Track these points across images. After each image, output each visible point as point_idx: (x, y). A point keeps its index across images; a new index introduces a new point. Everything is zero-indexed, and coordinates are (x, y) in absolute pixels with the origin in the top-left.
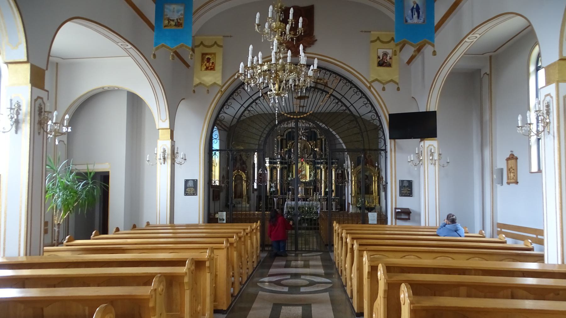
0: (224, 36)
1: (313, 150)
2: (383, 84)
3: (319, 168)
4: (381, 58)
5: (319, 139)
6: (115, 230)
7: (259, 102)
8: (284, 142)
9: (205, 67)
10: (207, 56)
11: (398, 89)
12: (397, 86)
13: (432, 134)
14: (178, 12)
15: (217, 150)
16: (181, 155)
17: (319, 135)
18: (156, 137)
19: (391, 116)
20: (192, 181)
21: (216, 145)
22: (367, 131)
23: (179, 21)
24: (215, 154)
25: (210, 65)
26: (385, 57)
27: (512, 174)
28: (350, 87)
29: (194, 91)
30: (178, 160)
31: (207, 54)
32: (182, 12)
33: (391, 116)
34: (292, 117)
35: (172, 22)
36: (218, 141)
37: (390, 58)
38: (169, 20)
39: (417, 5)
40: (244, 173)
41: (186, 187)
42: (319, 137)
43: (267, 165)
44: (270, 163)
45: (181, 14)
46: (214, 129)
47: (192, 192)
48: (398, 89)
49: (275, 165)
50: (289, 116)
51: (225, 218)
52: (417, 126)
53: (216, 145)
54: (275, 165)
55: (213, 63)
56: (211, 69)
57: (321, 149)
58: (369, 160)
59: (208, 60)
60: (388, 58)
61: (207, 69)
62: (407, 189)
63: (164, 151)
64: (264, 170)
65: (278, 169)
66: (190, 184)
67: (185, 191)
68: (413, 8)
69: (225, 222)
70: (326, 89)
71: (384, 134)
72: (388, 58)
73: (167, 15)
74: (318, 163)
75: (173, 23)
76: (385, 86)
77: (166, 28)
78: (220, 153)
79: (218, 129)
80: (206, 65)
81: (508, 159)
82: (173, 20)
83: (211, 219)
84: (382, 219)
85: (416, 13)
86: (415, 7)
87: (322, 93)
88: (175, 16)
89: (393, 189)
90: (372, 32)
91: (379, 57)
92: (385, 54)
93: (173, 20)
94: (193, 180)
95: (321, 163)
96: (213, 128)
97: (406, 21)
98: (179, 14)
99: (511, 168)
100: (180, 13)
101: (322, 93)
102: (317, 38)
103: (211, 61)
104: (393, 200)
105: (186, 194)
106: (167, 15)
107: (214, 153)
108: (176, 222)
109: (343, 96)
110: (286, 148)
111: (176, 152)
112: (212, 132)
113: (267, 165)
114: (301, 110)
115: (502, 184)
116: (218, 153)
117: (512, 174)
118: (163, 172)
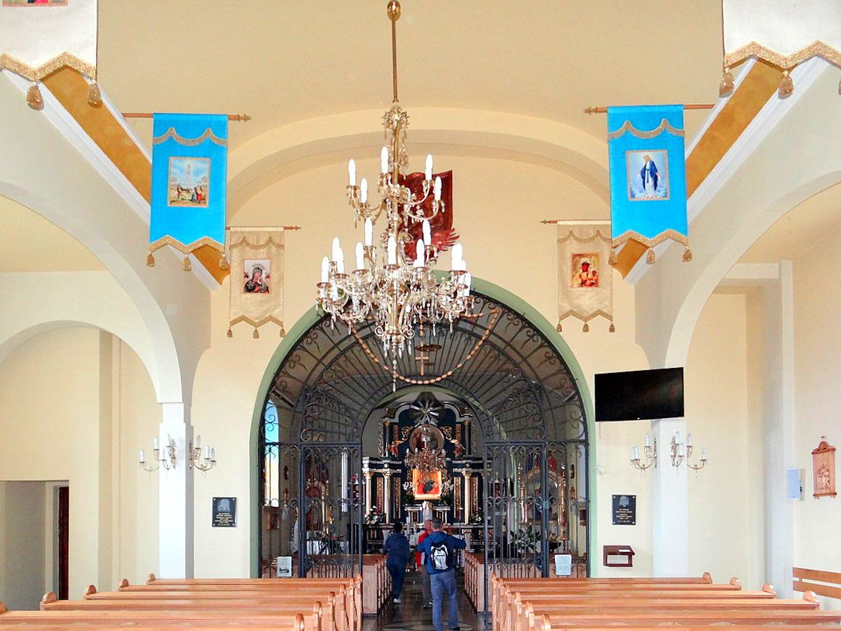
0: (285, 228)
1: (447, 442)
2: (586, 319)
3: (459, 475)
4: (251, 277)
5: (459, 423)
6: (87, 590)
7: (352, 355)
8: (396, 427)
9: (580, 281)
10: (583, 260)
11: (612, 329)
12: (609, 323)
13: (675, 409)
14: (197, 174)
15: (274, 444)
16: (205, 453)
17: (457, 415)
18: (158, 417)
19: (599, 378)
20: (228, 501)
21: (272, 435)
22: (551, 409)
23: (199, 192)
24: (270, 449)
25: (590, 276)
26: (257, 275)
27: (824, 479)
28: (520, 325)
29: (230, 334)
30: (198, 462)
31: (581, 256)
32: (206, 174)
33: (599, 378)
34: (414, 382)
35: (184, 193)
36: (277, 427)
37: (268, 277)
38: (180, 190)
39: (653, 164)
40: (324, 483)
41: (215, 512)
42: (458, 419)
43: (366, 470)
44: (371, 466)
45: (204, 179)
46: (268, 406)
47: (227, 521)
48: (612, 329)
49: (380, 471)
50: (408, 380)
51: (290, 568)
52: (644, 395)
53: (272, 435)
54: (380, 471)
55: (594, 273)
56: (592, 284)
57: (462, 441)
58: (555, 459)
59: (586, 267)
60: (264, 276)
61: (583, 283)
62: (625, 510)
63: (172, 447)
64: (360, 480)
65: (386, 477)
66: (224, 506)
67: (214, 518)
68: (645, 169)
69: (290, 574)
70: (477, 331)
71: (584, 414)
72: (264, 276)
73: (175, 180)
74: (457, 466)
75: (188, 196)
76: (588, 323)
77: (174, 205)
78: (279, 448)
79: (279, 407)
80: (580, 276)
81: (815, 452)
82: (188, 191)
83: (264, 565)
84: (582, 561)
85: (651, 180)
86: (648, 167)
87: (469, 339)
88: (191, 183)
89: (602, 511)
90: (559, 223)
91: (247, 276)
92: (259, 269)
93: (188, 191)
94: (230, 499)
95: (463, 466)
96: (266, 402)
97: (633, 196)
98: (199, 179)
99: (823, 467)
100: (201, 176)
101: (469, 339)
102: (456, 233)
103: (591, 270)
104: (604, 531)
105: (216, 523)
106: (175, 180)
107: (267, 448)
108: (198, 575)
109: (336, 345)
110: (400, 439)
111: (195, 446)
112: (264, 410)
113: (366, 470)
114: (431, 371)
115: (802, 499)
116: (275, 449)
117: (824, 479)
118: (172, 481)
